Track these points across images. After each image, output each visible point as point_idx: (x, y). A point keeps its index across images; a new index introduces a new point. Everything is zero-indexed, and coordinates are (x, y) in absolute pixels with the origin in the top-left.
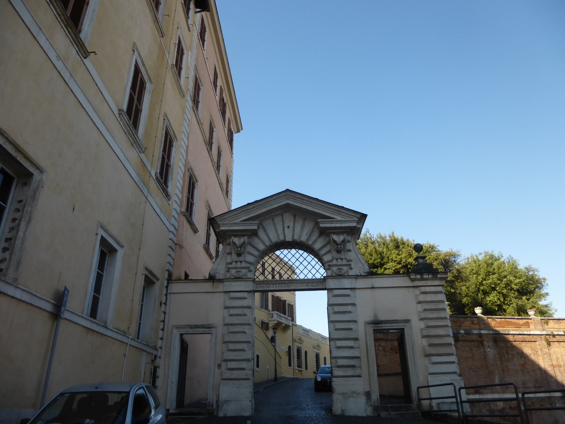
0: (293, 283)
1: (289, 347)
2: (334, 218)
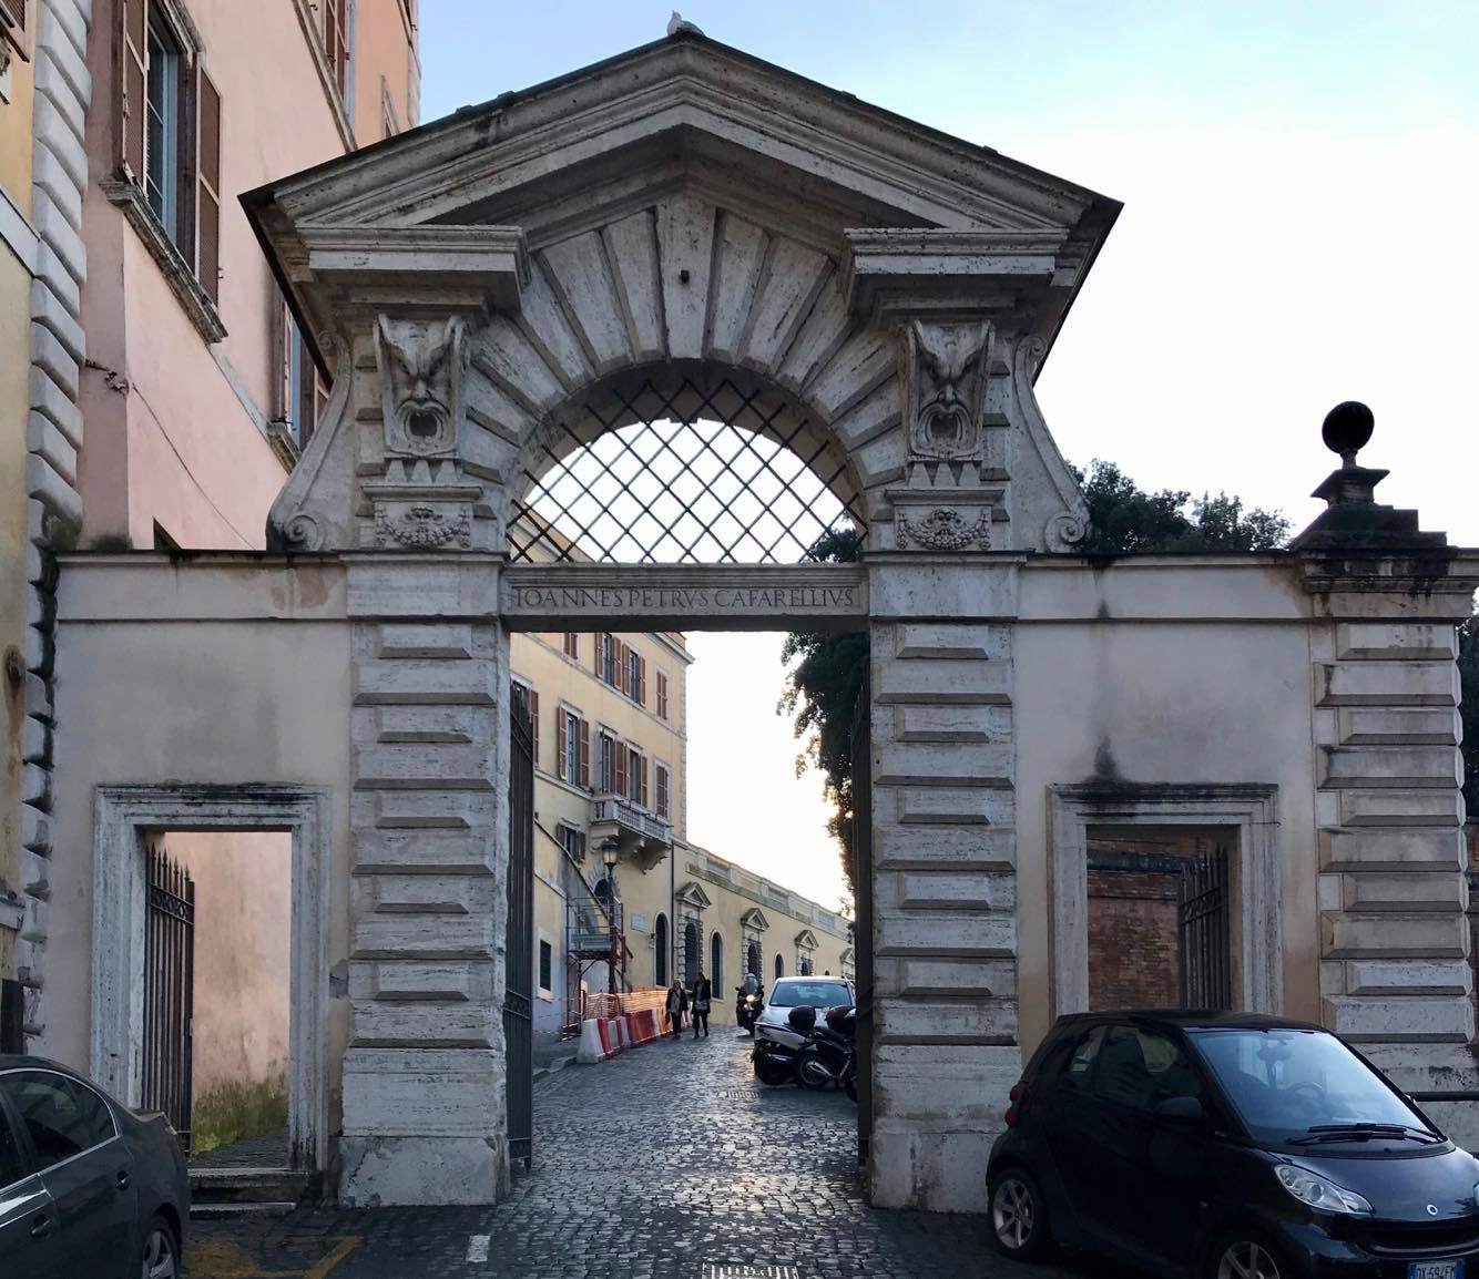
0: (704, 586)
1: (661, 919)
2: (933, 225)
